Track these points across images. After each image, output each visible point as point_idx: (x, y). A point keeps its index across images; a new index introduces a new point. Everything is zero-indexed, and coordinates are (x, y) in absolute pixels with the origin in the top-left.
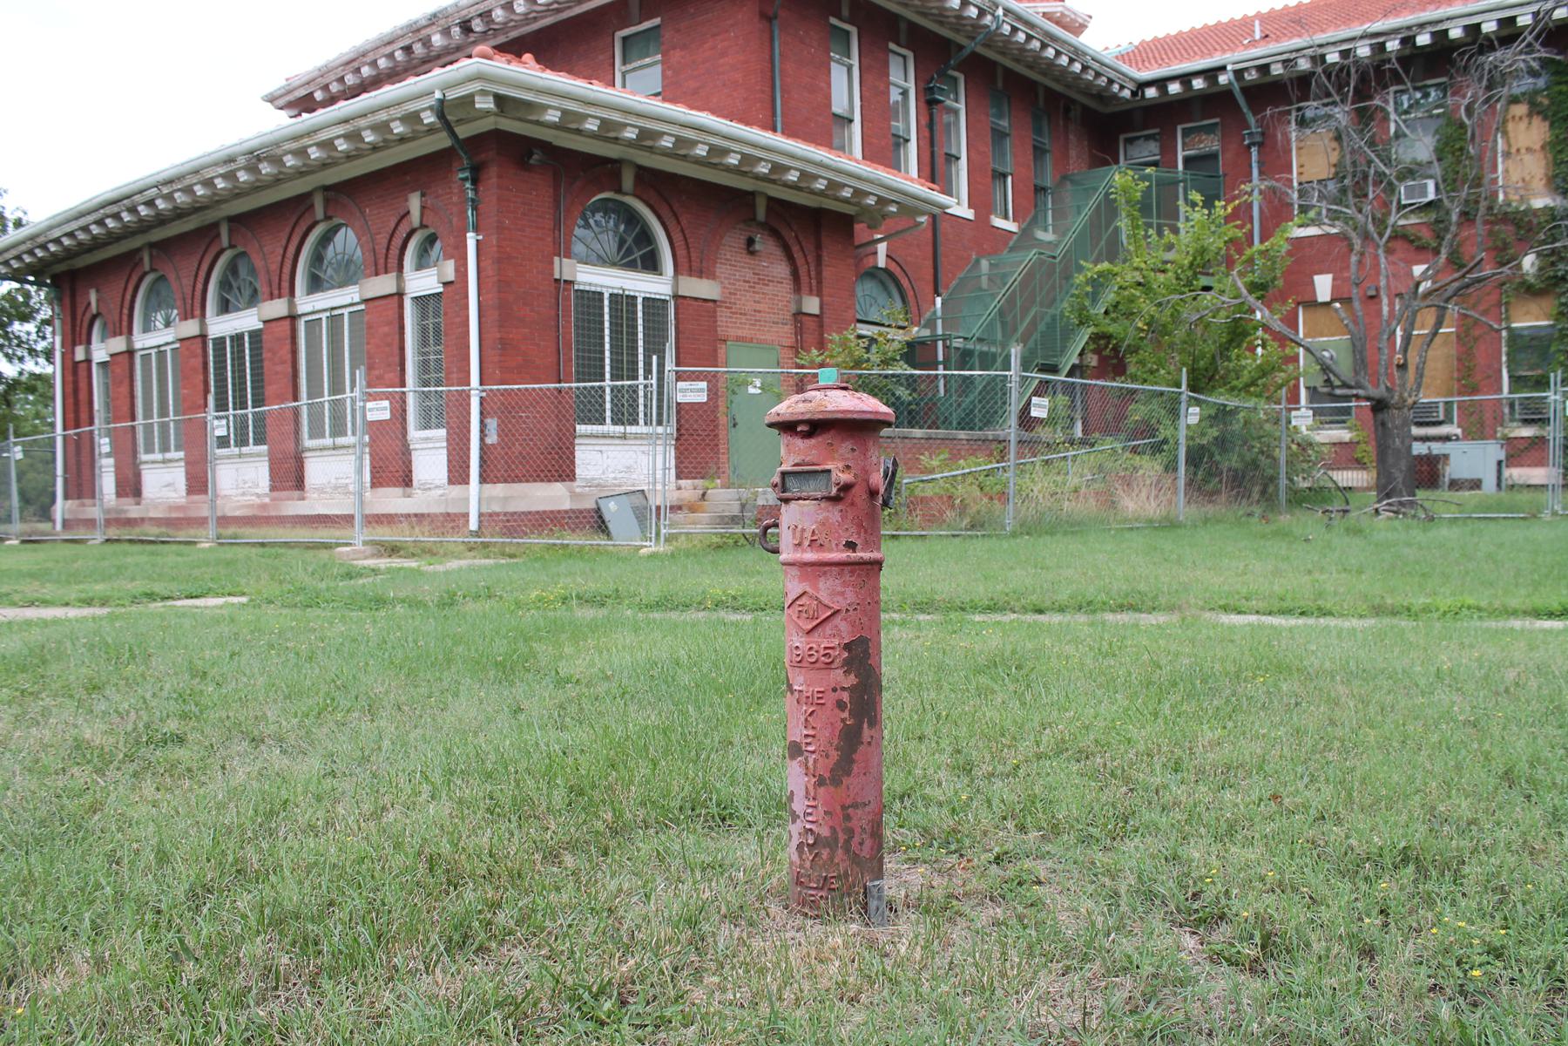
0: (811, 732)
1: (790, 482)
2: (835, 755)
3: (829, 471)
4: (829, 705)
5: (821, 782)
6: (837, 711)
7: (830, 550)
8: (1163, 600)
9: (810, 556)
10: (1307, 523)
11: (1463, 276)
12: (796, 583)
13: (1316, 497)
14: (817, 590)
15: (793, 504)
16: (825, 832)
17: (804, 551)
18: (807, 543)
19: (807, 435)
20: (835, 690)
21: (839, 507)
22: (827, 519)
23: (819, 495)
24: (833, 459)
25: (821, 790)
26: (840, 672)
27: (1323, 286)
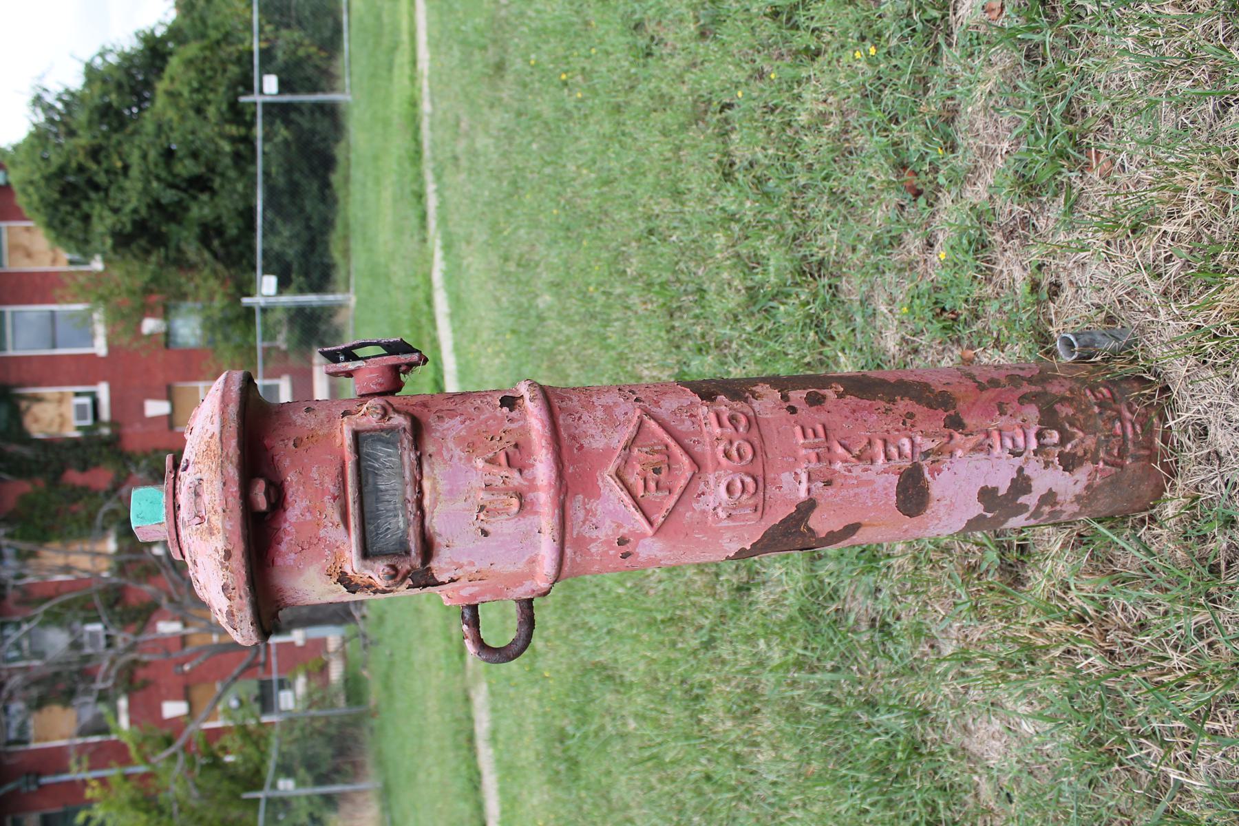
0: (879, 447)
1: (388, 540)
2: (903, 405)
3: (356, 435)
4: (823, 417)
5: (955, 423)
6: (828, 405)
7: (525, 431)
8: (460, 714)
9: (543, 468)
10: (375, 694)
11: (165, 567)
12: (597, 506)
13: (354, 688)
14: (608, 452)
15: (435, 523)
16: (1032, 413)
17: (533, 487)
18: (516, 479)
19: (278, 500)
20: (792, 410)
21: (432, 420)
22: (460, 440)
23: (409, 457)
24: (329, 437)
25: (970, 422)
26: (756, 404)
27: (173, 709)
